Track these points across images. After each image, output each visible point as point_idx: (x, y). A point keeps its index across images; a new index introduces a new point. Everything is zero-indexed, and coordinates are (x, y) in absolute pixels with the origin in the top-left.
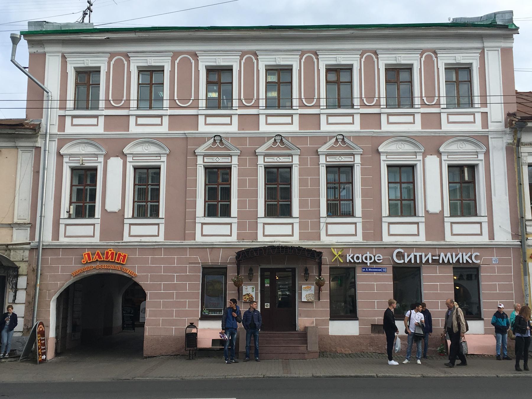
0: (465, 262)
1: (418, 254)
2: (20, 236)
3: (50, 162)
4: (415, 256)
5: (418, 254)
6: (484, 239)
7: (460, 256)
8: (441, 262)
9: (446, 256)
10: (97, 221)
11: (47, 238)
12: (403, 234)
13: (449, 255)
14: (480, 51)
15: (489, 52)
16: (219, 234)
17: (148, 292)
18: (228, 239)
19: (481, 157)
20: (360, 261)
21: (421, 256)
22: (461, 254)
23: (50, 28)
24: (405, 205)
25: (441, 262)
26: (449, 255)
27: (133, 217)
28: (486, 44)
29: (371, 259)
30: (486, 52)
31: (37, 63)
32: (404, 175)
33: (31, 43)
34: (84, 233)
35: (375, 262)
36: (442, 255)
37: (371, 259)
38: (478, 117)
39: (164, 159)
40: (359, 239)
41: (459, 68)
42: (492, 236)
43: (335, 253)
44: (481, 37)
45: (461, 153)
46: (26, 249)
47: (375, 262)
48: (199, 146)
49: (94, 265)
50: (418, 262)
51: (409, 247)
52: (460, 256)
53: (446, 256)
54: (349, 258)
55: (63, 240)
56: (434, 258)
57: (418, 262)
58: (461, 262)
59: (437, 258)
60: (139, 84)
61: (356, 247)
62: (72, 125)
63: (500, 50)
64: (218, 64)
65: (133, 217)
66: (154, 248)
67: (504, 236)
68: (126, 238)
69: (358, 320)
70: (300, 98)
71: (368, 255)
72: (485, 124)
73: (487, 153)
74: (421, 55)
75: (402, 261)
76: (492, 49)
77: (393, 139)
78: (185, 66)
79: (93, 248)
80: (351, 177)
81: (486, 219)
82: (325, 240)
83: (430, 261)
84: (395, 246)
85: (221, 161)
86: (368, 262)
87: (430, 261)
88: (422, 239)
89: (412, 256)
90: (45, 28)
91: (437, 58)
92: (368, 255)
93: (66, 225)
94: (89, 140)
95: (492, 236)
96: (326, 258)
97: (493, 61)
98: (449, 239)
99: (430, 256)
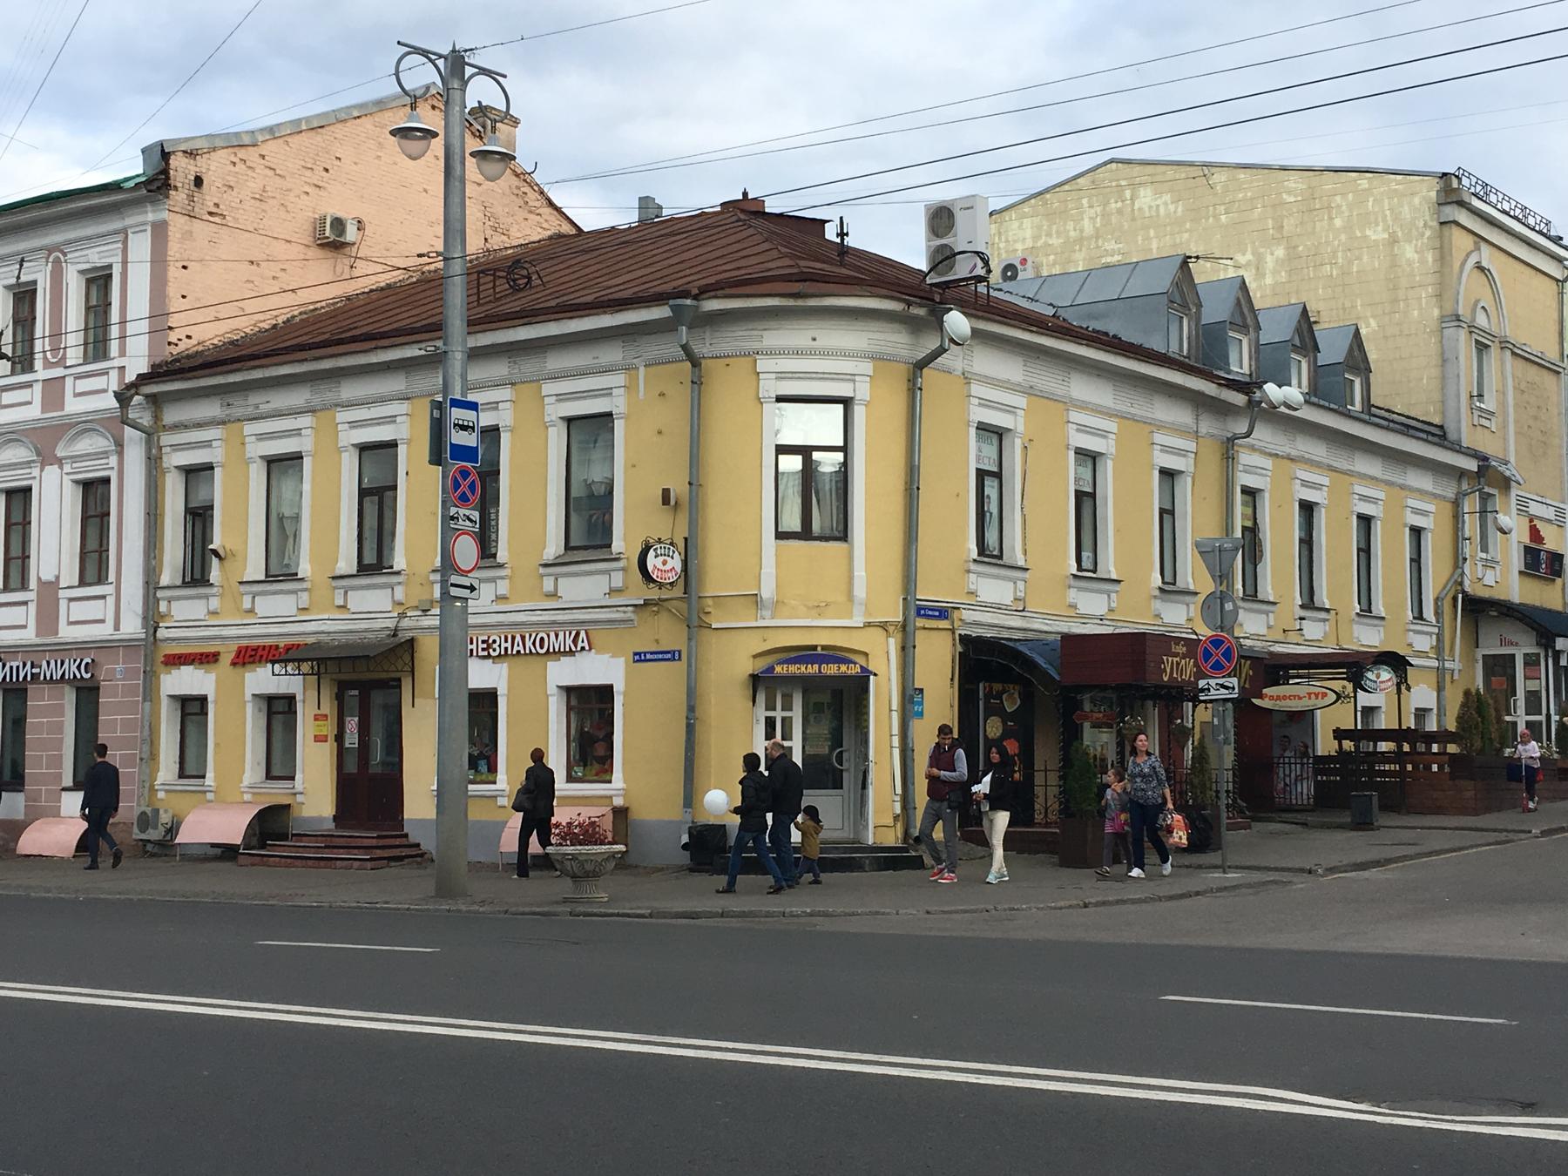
1: (15, 664)
7: (66, 665)
42: (117, 628)
67: (132, 626)
73: (120, 454)
88: (29, 636)
95: (117, 628)
97: (141, 246)
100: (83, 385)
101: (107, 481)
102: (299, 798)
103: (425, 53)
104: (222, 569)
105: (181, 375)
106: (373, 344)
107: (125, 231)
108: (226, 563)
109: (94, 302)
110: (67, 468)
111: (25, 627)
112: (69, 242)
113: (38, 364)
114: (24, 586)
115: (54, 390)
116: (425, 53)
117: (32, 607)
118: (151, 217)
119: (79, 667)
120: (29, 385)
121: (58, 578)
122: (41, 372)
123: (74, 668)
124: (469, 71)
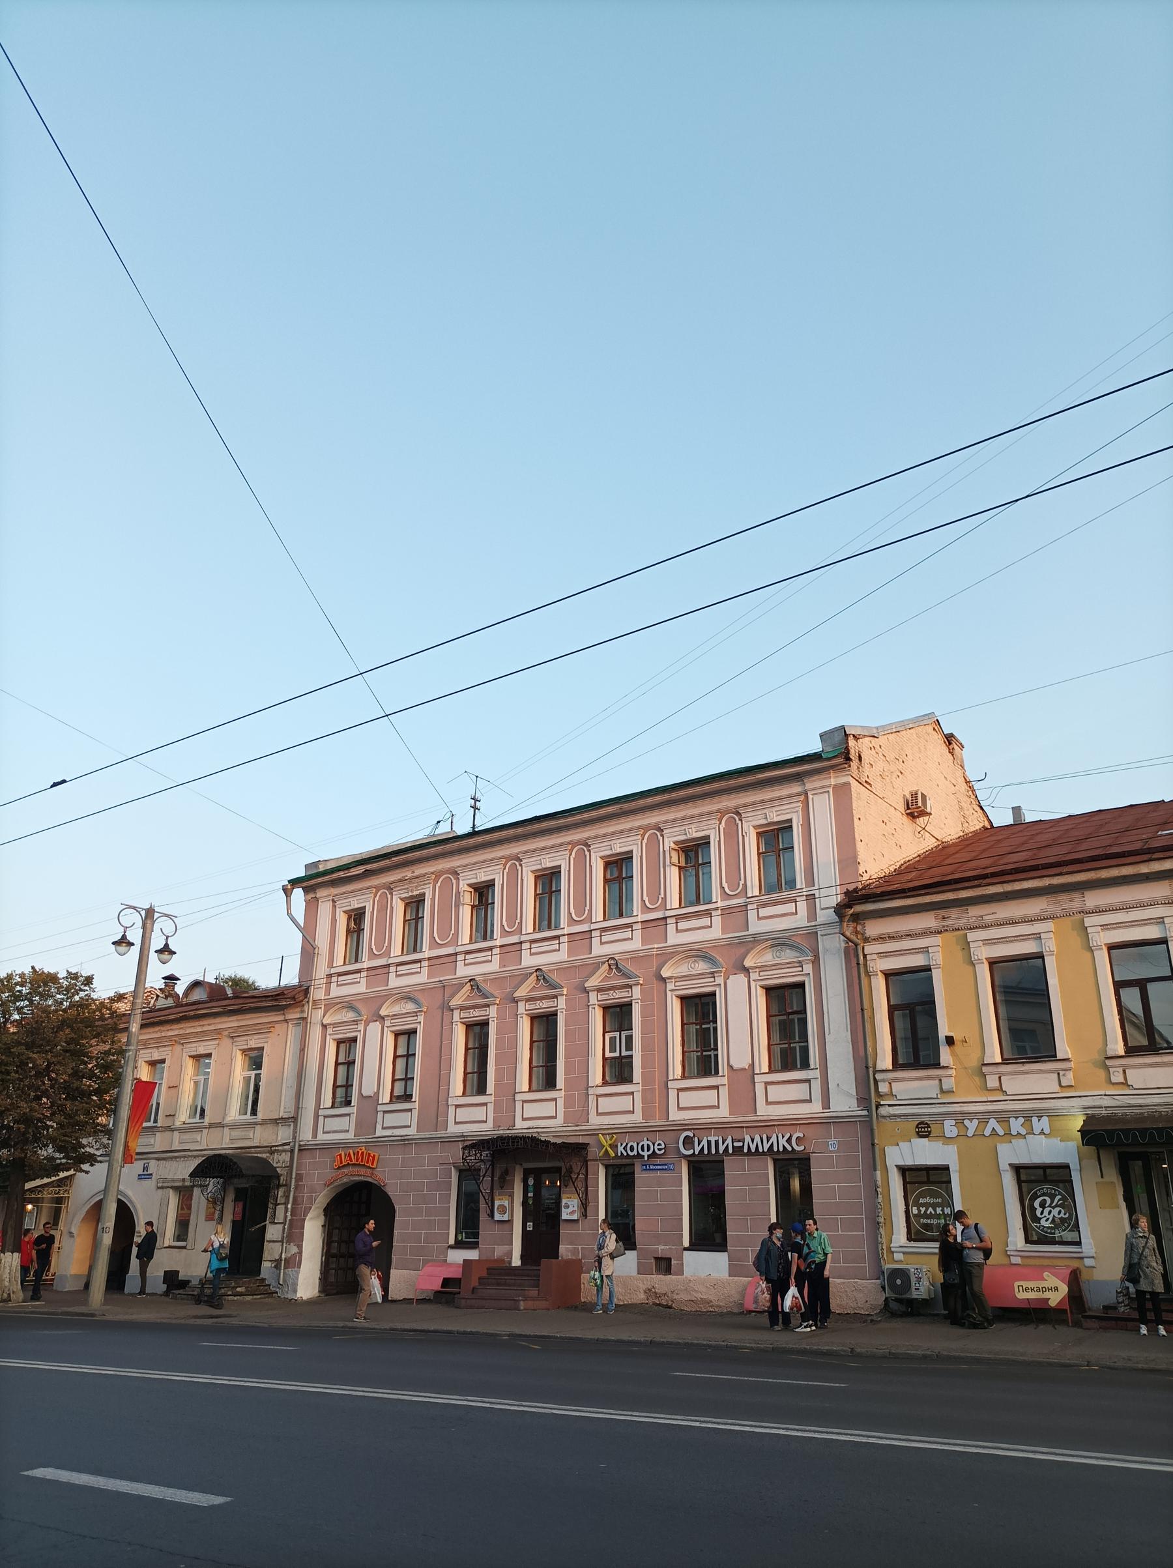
0: (781, 1149)
1: (713, 1139)
2: (283, 1135)
3: (315, 1033)
4: (709, 1142)
5: (713, 1139)
6: (816, 1108)
7: (774, 1139)
8: (746, 1150)
9: (753, 1140)
10: (722, 1080)
11: (306, 1135)
12: (700, 1104)
13: (757, 1139)
14: (802, 798)
15: (816, 798)
16: (475, 1119)
17: (397, 1207)
18: (483, 1127)
19: (808, 968)
20: (635, 1153)
21: (717, 1142)
22: (774, 1136)
23: (330, 866)
24: (703, 1058)
25: (746, 1150)
26: (757, 1139)
27: (684, 1077)
28: (808, 786)
29: (649, 1149)
30: (810, 797)
31: (311, 907)
32: (701, 1009)
33: (307, 890)
34: (341, 1128)
35: (654, 1155)
36: (748, 1139)
37: (649, 1149)
38: (802, 906)
39: (421, 1019)
40: (637, 1118)
41: (779, 829)
42: (826, 1104)
43: (604, 1142)
44: (798, 777)
45: (785, 969)
46: (285, 1151)
47: (654, 1155)
48: (453, 996)
49: (345, 1170)
50: (713, 1151)
51: (707, 1128)
52: (774, 1139)
53: (753, 1140)
54: (620, 1149)
55: (321, 1137)
56: (736, 1144)
57: (713, 1151)
58: (775, 1149)
59: (740, 1144)
60: (759, 854)
61: (634, 1131)
62: (677, 931)
63: (831, 791)
64: (479, 880)
65: (684, 1077)
66: (405, 1142)
67: (844, 1103)
68: (380, 1132)
69: (634, 1249)
70: (502, 926)
71: (645, 1143)
72: (812, 915)
73: (816, 961)
74: (643, 836)
75: (691, 1152)
76: (822, 790)
77: (770, 943)
78: (654, 844)
79: (346, 1145)
80: (997, 983)
81: (817, 1073)
82: (595, 1121)
83: (730, 1151)
84: (684, 1126)
85: (619, 996)
86: (646, 1154)
87: (730, 1151)
88: (724, 1113)
89: (704, 1143)
90: (322, 868)
91: (391, 894)
92: (645, 1143)
93: (680, 1090)
94: (700, 953)
95: (826, 1104)
96: (593, 1152)
97: (822, 807)
98: (764, 1111)
99: (729, 1141)
100: (537, 947)
101: (801, 985)
102: (1088, 1262)
103: (134, 908)
104: (953, 1054)
105: (860, 903)
106: (1146, 857)
107: (806, 793)
108: (958, 1046)
109: (408, 917)
110: (387, 1023)
111: (555, 1117)
112: (663, 822)
113: (564, 921)
114: (348, 1103)
115: (736, 914)
116: (134, 908)
117: (491, 1107)
118: (833, 781)
119: (789, 1141)
120: (359, 971)
121: (752, 1065)
122: (366, 963)
123: (783, 1142)
124: (156, 915)
